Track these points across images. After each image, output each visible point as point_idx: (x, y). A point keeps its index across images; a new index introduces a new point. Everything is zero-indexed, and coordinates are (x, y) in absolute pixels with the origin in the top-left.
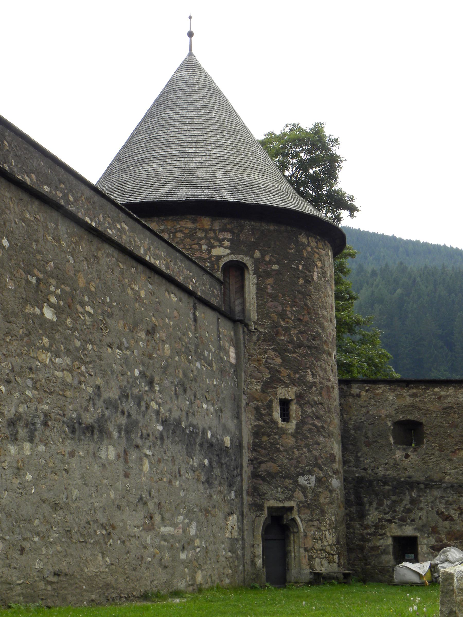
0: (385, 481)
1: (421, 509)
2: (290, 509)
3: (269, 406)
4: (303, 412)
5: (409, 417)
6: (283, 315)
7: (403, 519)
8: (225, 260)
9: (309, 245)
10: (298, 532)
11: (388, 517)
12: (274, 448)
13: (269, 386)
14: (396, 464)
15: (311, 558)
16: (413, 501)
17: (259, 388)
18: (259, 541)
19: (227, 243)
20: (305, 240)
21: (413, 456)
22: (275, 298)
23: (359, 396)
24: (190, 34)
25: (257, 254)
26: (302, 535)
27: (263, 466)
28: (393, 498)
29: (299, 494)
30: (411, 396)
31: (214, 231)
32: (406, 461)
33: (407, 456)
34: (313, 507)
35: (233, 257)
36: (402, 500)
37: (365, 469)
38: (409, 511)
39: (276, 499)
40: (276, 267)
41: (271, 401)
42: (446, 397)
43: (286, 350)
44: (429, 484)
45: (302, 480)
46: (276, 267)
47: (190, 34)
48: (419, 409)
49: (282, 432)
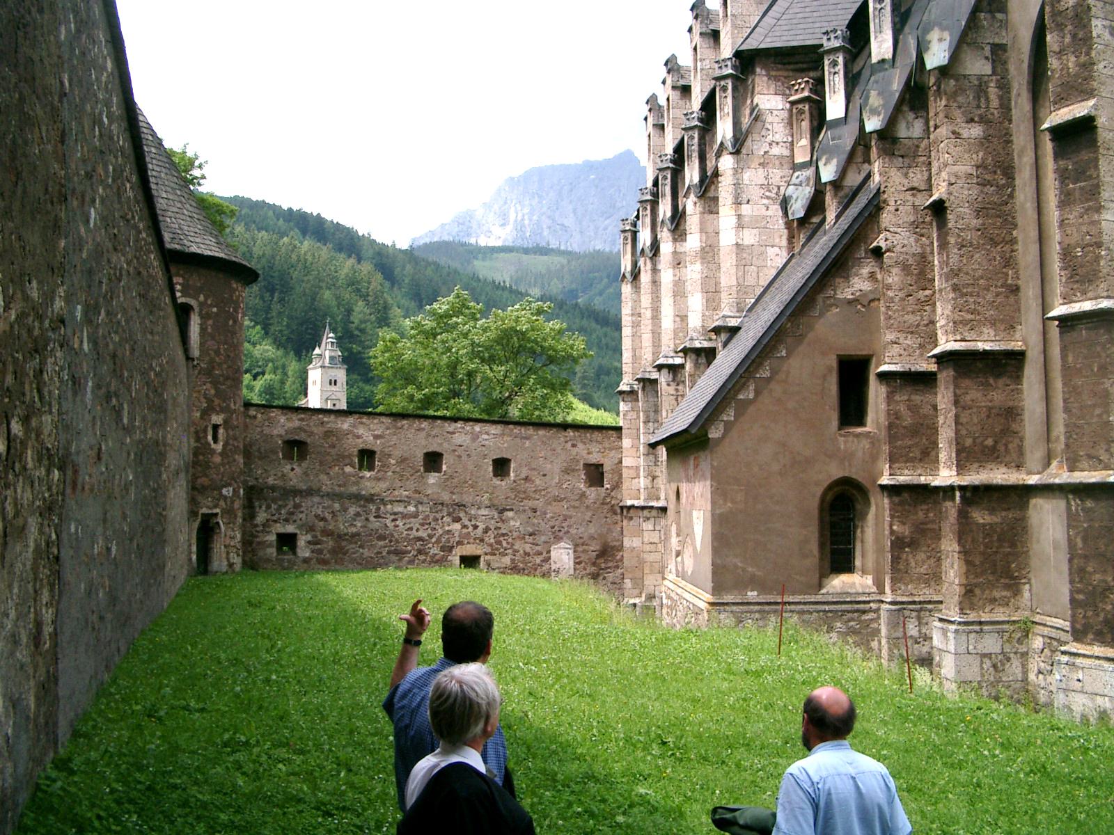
0: (273, 488)
1: (302, 512)
2: (216, 515)
3: (205, 431)
4: (228, 434)
5: (297, 438)
6: (217, 352)
7: (286, 520)
9: (237, 289)
10: (220, 533)
11: (275, 518)
12: (207, 465)
13: (206, 413)
14: (284, 475)
15: (228, 553)
17: (198, 415)
18: (194, 541)
20: (235, 286)
21: (297, 469)
23: (255, 417)
25: (202, 298)
26: (223, 535)
27: (199, 481)
28: (280, 503)
29: (222, 503)
30: (299, 420)
32: (294, 473)
33: (293, 469)
36: (287, 505)
37: (256, 479)
38: (292, 513)
40: (215, 310)
41: (206, 427)
44: (310, 492)
45: (224, 491)
46: (215, 310)
48: (305, 431)
49: (213, 452)
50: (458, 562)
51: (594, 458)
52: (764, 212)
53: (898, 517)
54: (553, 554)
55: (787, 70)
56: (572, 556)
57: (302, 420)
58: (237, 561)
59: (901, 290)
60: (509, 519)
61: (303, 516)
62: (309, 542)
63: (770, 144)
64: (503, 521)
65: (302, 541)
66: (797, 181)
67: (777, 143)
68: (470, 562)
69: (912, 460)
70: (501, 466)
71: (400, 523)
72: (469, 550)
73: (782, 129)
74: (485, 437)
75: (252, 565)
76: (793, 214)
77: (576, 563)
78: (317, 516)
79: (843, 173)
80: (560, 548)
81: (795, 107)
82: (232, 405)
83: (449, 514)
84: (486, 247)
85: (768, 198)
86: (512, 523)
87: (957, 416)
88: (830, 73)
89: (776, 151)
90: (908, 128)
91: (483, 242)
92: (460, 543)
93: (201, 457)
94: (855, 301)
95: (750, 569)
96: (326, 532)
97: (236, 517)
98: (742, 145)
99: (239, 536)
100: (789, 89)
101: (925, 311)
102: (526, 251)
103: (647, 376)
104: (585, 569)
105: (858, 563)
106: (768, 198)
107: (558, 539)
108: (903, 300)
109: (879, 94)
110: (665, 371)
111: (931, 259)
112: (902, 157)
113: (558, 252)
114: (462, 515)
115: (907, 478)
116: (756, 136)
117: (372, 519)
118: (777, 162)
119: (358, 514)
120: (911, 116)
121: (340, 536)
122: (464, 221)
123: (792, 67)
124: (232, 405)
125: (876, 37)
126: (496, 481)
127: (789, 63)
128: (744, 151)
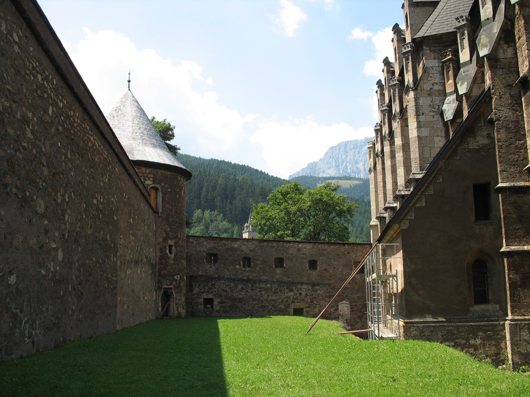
0: (201, 276)
2: (171, 288)
6: (171, 210)
7: (208, 292)
8: (151, 186)
11: (202, 291)
13: (165, 239)
14: (206, 270)
15: (178, 307)
16: (212, 285)
17: (161, 240)
18: (160, 301)
19: (151, 179)
23: (192, 242)
24: (129, 81)
25: (163, 184)
27: (162, 272)
29: (174, 283)
31: (147, 173)
32: (211, 269)
34: (178, 287)
35: (154, 185)
38: (211, 288)
39: (167, 285)
40: (169, 190)
41: (166, 246)
42: (227, 244)
44: (219, 278)
45: (175, 277)
46: (169, 190)
47: (129, 81)
48: (216, 249)
49: (169, 258)
50: (292, 312)
52: (432, 119)
53: (513, 270)
54: (339, 307)
55: (439, 47)
56: (349, 307)
57: (215, 243)
58: (183, 312)
59: (506, 142)
60: (317, 290)
61: (216, 290)
62: (219, 302)
63: (433, 84)
64: (314, 291)
65: (215, 302)
66: (448, 102)
67: (437, 84)
69: (519, 237)
70: (313, 264)
71: (263, 293)
72: (297, 305)
73: (439, 76)
74: (305, 250)
75: (192, 314)
76: (447, 118)
77: (351, 311)
78: (223, 290)
79: (471, 89)
80: (343, 304)
82: (179, 236)
83: (287, 288)
84: (323, 177)
85: (433, 112)
86: (319, 292)
89: (436, 87)
90: (504, 53)
91: (321, 175)
92: (293, 302)
93: (163, 261)
94: (478, 151)
95: (427, 303)
96: (227, 298)
97: (182, 290)
98: (418, 85)
99: (183, 299)
100: (441, 56)
101: (521, 152)
102: (340, 178)
103: (382, 215)
104: (356, 314)
105: (491, 297)
106: (433, 112)
107: (342, 299)
108: (507, 146)
109: (486, 36)
110: (389, 210)
111: (522, 123)
112: (502, 69)
113: (355, 179)
114: (294, 288)
115: (516, 247)
116: (425, 81)
117: (249, 291)
118: (437, 94)
119: (243, 289)
120: (505, 46)
121: (234, 299)
122: (312, 166)
124: (179, 236)
125: (483, 8)
127: (440, 43)
128: (419, 88)
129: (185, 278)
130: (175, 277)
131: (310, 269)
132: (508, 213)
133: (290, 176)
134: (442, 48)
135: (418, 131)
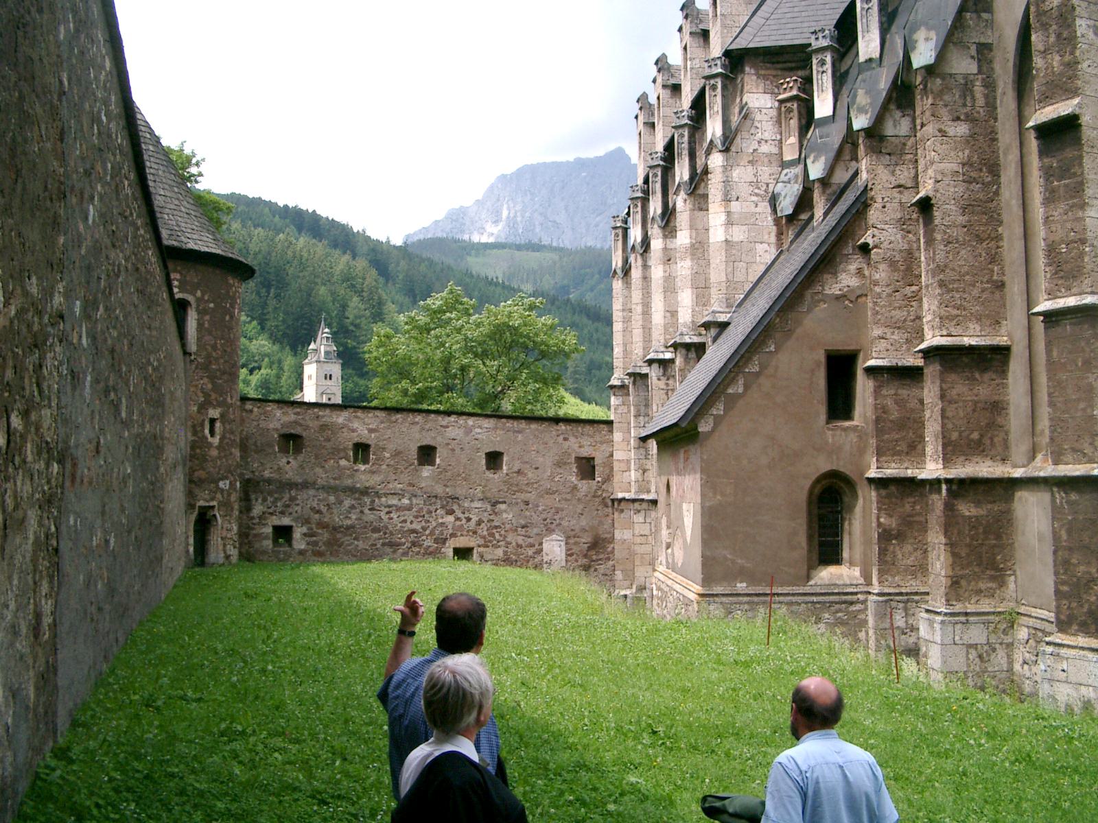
0: (269, 481)
1: (298, 505)
2: (213, 507)
3: (202, 425)
4: (225, 428)
5: (292, 431)
6: (214, 347)
7: (282, 513)
10: (217, 525)
11: (271, 511)
12: (204, 459)
13: (203, 407)
14: (279, 469)
15: (225, 545)
17: (195, 409)
20: (231, 282)
22: (210, 333)
23: (251, 411)
25: (199, 294)
26: (220, 527)
27: (196, 474)
28: (276, 495)
29: (219, 496)
32: (289, 466)
37: (253, 472)
38: (288, 506)
40: (212, 305)
41: (204, 421)
43: (216, 377)
44: (305, 485)
45: (221, 484)
46: (212, 305)
48: (301, 425)
49: (210, 445)
50: (451, 554)
51: (585, 452)
52: (753, 209)
55: (776, 69)
56: (564, 548)
57: (297, 414)
59: (888, 286)
60: (501, 512)
61: (298, 508)
62: (305, 535)
63: (759, 142)
65: (297, 534)
66: (786, 179)
67: (766, 141)
68: (463, 553)
69: (899, 453)
70: (494, 459)
71: (394, 515)
72: (462, 542)
73: (771, 127)
74: (478, 430)
75: (248, 557)
76: (781, 211)
77: (568, 555)
78: (312, 509)
79: (831, 171)
81: (783, 105)
83: (442, 507)
84: (479, 244)
85: (757, 195)
86: (505, 515)
87: (943, 410)
88: (818, 72)
89: (765, 148)
90: (895, 126)
91: (476, 238)
92: (453, 535)
95: (739, 561)
96: (321, 525)
97: (232, 509)
98: (731, 143)
100: (778, 88)
101: (912, 306)
104: (577, 561)
106: (757, 195)
107: (550, 531)
109: (866, 93)
110: (655, 366)
111: (917, 255)
112: (889, 154)
114: (455, 507)
115: (894, 471)
117: (366, 511)
118: (766, 160)
119: (352, 507)
120: (898, 114)
121: (335, 529)
122: (458, 216)
123: (780, 66)
124: (229, 399)
125: (863, 37)
126: (489, 474)
127: (778, 63)
128: (733, 149)
129: (238, 484)
130: (221, 484)
131: (488, 468)
132: (884, 412)
133: (408, 236)
134: (779, 73)
135: (726, 231)
